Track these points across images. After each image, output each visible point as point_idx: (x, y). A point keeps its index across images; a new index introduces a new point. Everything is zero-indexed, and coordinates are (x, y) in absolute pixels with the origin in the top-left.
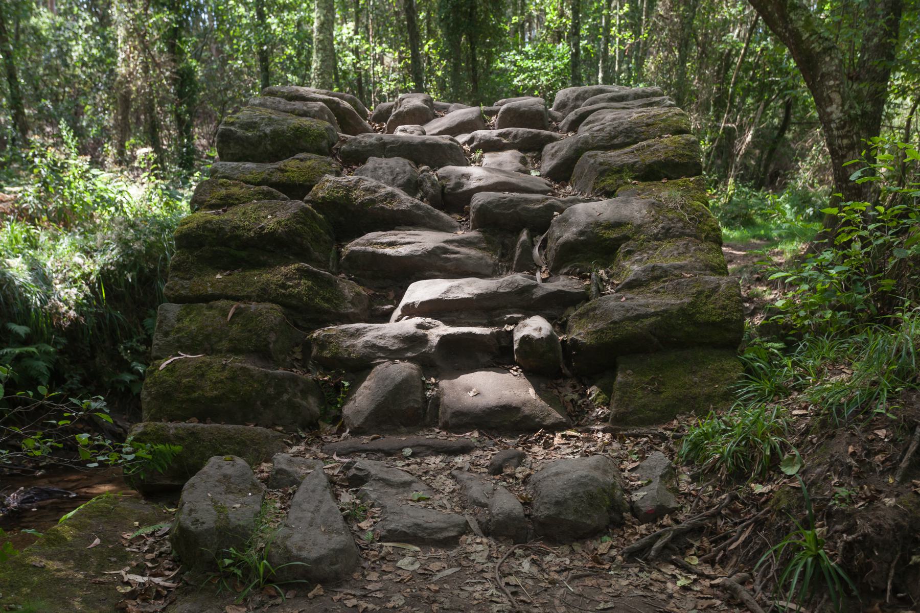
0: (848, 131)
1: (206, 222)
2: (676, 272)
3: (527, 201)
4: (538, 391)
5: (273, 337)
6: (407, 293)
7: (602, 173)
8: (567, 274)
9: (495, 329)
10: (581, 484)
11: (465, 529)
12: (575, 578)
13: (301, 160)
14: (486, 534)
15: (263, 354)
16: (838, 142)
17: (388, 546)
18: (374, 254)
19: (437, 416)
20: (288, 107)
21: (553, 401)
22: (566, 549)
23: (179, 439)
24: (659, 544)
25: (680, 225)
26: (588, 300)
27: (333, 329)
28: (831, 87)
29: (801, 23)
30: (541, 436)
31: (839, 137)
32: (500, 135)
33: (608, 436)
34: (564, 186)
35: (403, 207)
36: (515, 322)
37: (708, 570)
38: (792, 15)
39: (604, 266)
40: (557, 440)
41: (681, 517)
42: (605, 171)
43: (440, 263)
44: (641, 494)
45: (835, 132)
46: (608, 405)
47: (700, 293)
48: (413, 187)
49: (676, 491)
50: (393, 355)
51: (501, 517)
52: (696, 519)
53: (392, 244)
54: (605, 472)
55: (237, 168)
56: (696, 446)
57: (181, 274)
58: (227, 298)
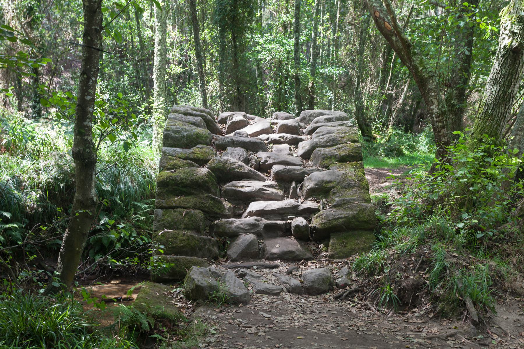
0: (441, 119)
1: (170, 176)
2: (352, 201)
3: (295, 170)
4: (301, 245)
5: (201, 223)
6: (250, 206)
7: (323, 158)
8: (311, 200)
9: (284, 222)
10: (320, 276)
11: (282, 290)
12: (319, 304)
13: (200, 148)
14: (289, 292)
15: (197, 230)
16: (436, 124)
17: (258, 295)
18: (236, 191)
19: (264, 255)
20: (187, 120)
21: (308, 249)
22: (315, 297)
23: (172, 261)
24: (345, 294)
25: (353, 182)
26: (319, 211)
27: (222, 220)
28: (433, 96)
29: (418, 62)
30: (303, 263)
31: (437, 121)
32: (280, 137)
33: (327, 262)
34: (307, 161)
35: (246, 171)
36: (292, 219)
37: (360, 302)
38: (413, 58)
39: (325, 198)
40: (309, 263)
41: (352, 287)
42: (325, 157)
43: (261, 195)
44: (339, 280)
45: (435, 119)
46: (327, 251)
47: (360, 210)
48: (247, 161)
49: (351, 279)
50: (247, 231)
51: (294, 286)
52: (356, 287)
53: (242, 187)
54: (327, 273)
55: (175, 151)
56: (358, 265)
57: (161, 198)
58: (181, 207)
